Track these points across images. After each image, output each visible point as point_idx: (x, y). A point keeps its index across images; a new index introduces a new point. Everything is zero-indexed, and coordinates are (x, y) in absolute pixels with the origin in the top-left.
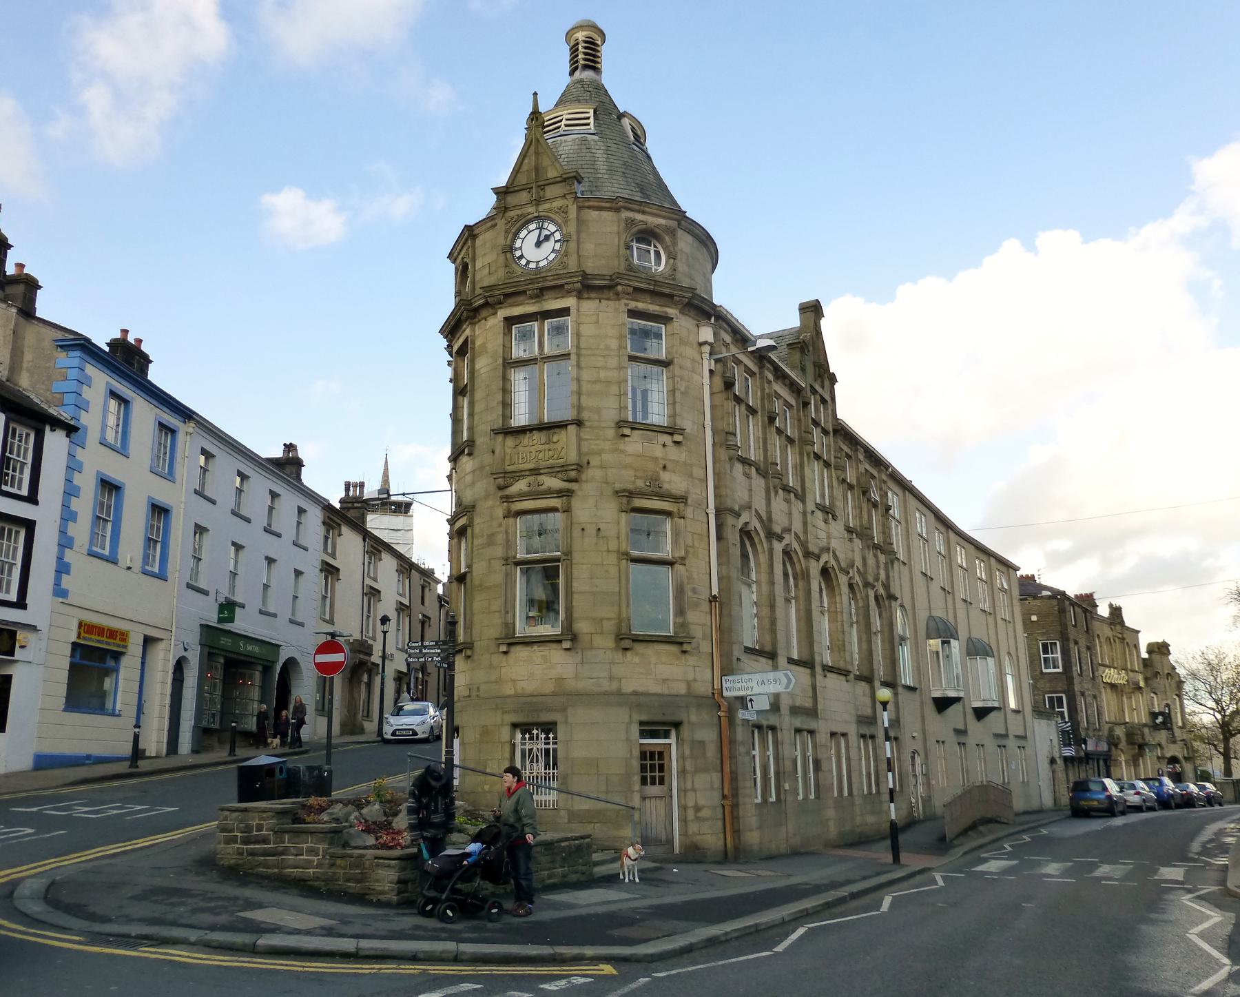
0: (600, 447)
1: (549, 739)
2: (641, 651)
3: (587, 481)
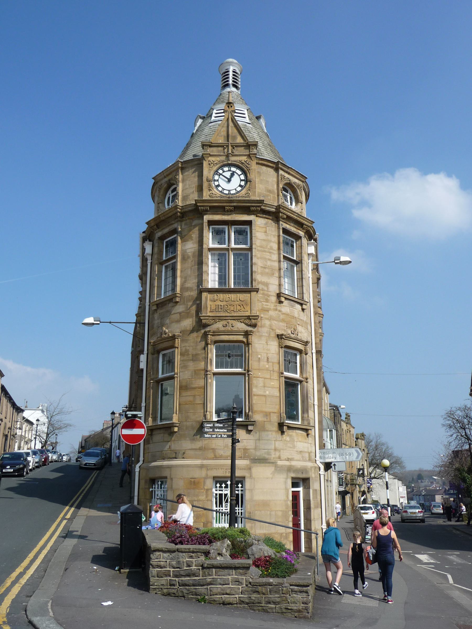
0: (268, 307)
1: (222, 487)
2: (290, 433)
3: (261, 327)
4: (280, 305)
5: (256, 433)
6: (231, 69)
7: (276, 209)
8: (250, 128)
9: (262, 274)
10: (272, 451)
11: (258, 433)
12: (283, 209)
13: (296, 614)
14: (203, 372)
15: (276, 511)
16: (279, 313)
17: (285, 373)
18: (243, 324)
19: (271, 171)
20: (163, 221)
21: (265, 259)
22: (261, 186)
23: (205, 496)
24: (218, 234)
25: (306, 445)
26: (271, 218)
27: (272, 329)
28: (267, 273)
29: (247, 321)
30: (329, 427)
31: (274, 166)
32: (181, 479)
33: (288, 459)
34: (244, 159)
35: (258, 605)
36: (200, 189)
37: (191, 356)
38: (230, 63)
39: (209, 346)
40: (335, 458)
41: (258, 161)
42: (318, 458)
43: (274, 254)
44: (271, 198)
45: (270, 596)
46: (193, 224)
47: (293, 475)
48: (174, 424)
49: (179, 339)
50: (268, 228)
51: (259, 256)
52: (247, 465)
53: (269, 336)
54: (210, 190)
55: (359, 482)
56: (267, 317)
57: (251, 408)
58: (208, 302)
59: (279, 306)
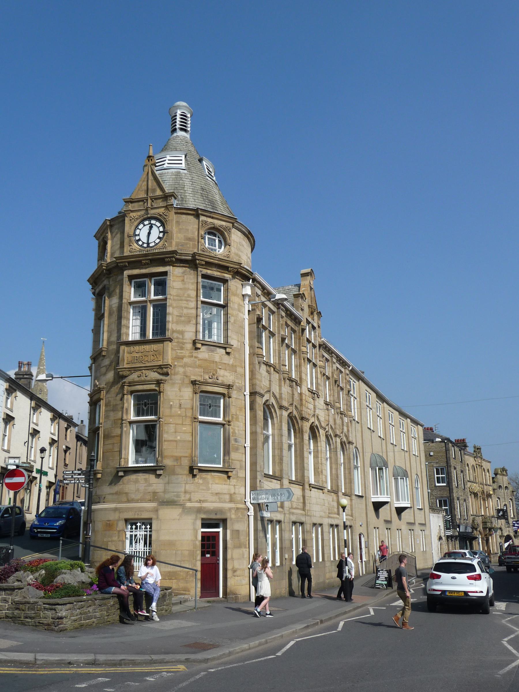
0: (183, 354)
2: (204, 476)
3: (174, 374)
4: (196, 351)
5: (166, 477)
6: (179, 112)
7: (192, 257)
8: (183, 175)
9: (177, 323)
10: (182, 494)
11: (167, 477)
12: (199, 256)
13: (46, 627)
14: (120, 421)
15: (182, 550)
16: (195, 359)
17: (200, 417)
18: (156, 374)
19: (191, 218)
20: (97, 278)
21: (181, 308)
22: (179, 235)
23: (117, 537)
24: (141, 288)
25: (226, 487)
26: (188, 265)
27: (186, 376)
28: (183, 321)
29: (159, 370)
30: (378, 464)
31: (194, 213)
32: (100, 521)
33: (200, 500)
34: (161, 211)
35: (19, 619)
36: (122, 246)
37: (112, 406)
38: (178, 107)
39: (125, 396)
40: (268, 499)
41: (176, 211)
42: (248, 499)
43: (192, 301)
44: (190, 246)
45: (28, 612)
46: (118, 280)
47: (204, 516)
48: (97, 471)
49: (105, 391)
50: (185, 277)
51: (175, 305)
52: (155, 507)
53: (183, 383)
54: (131, 245)
55: (494, 525)
56: (181, 364)
57: (160, 453)
58: (125, 354)
59: (195, 352)
